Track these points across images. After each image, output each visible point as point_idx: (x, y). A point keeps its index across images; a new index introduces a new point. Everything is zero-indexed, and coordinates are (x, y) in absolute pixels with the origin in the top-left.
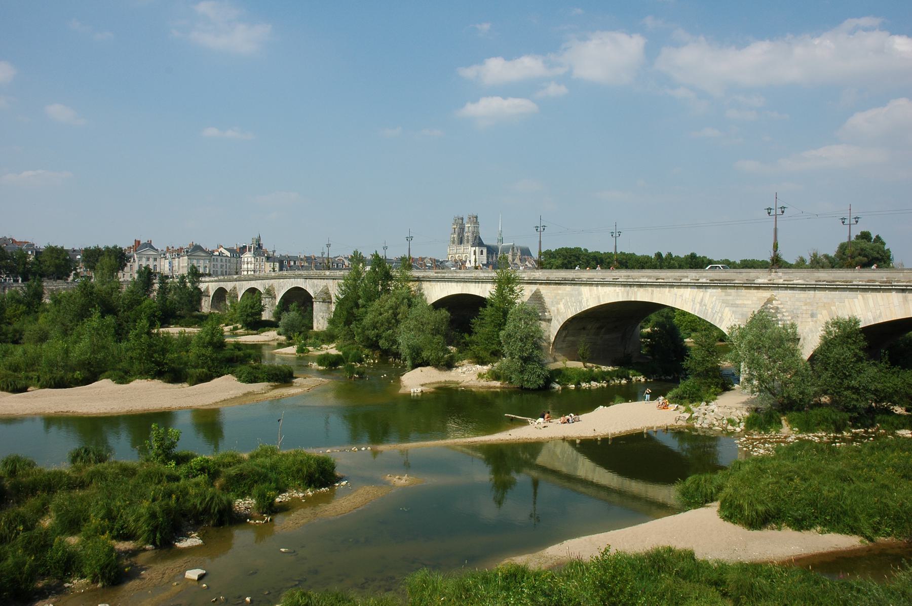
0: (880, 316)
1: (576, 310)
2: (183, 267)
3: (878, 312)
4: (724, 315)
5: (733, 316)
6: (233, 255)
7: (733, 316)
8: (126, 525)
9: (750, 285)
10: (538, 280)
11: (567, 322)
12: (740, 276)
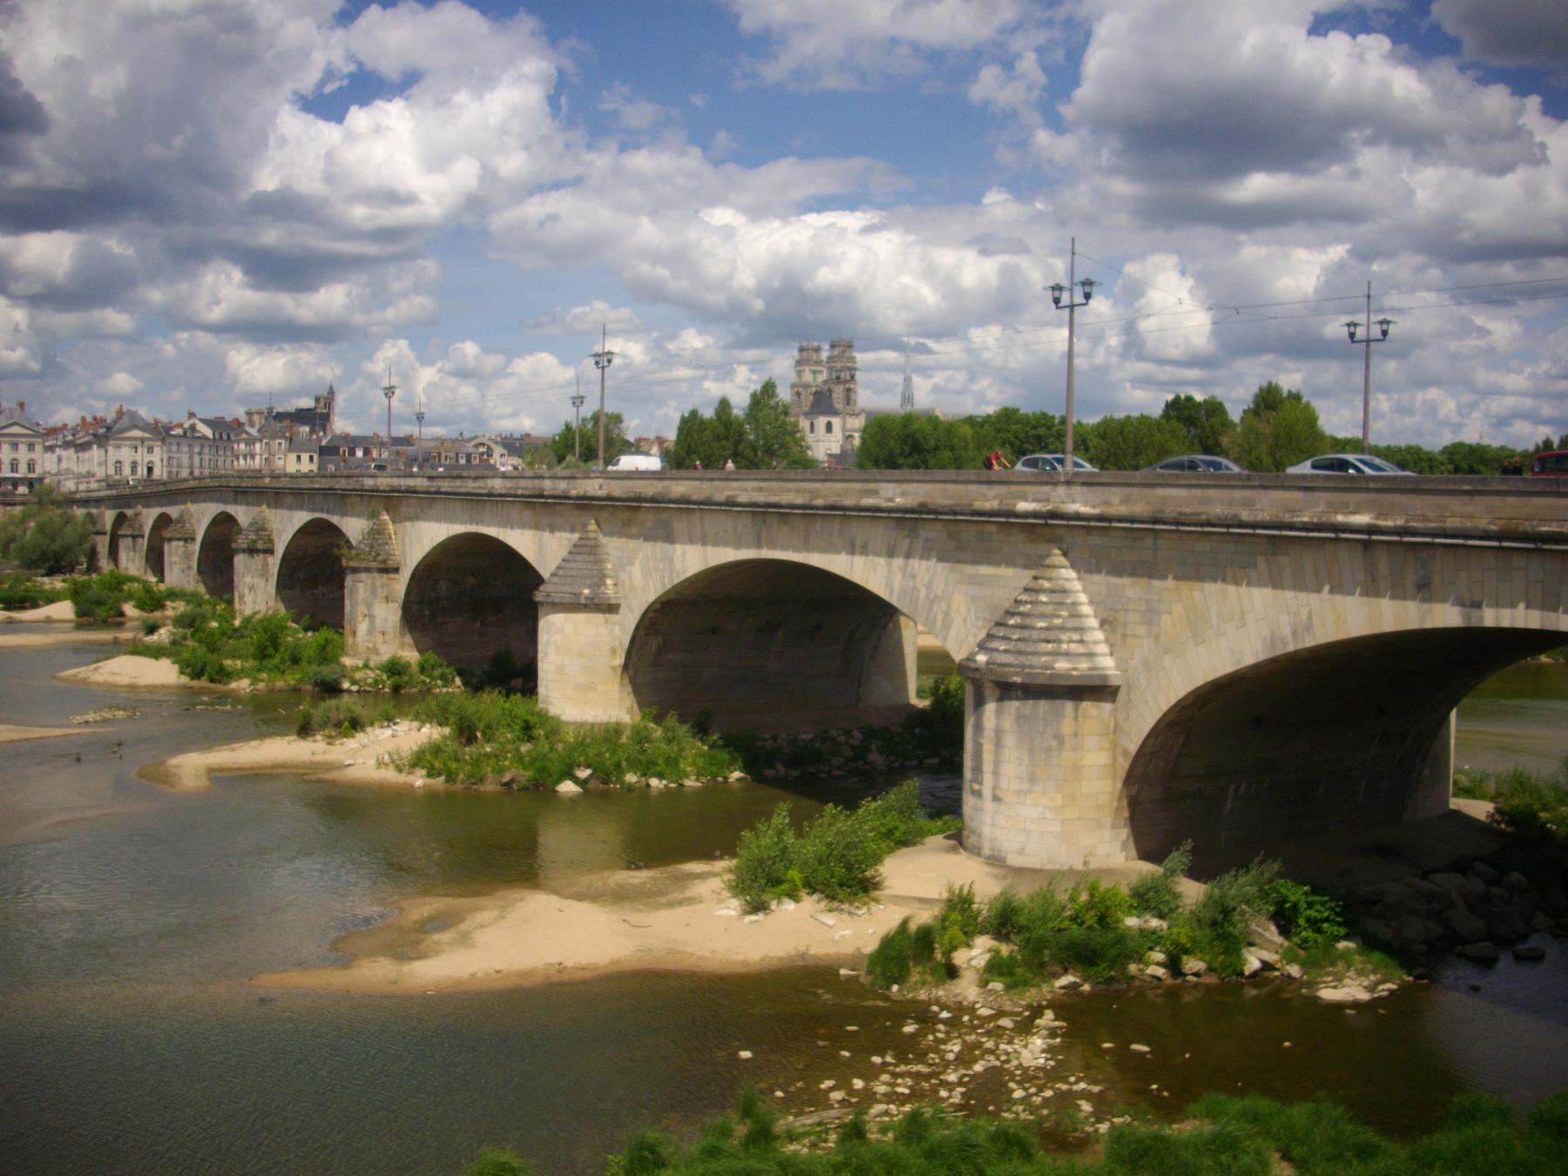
0: (1309, 627)
1: (663, 583)
2: (978, 476)
3: (1304, 614)
4: (954, 606)
5: (972, 610)
6: (221, 435)
7: (972, 610)
8: (113, 950)
9: (1428, 540)
10: (968, 521)
11: (651, 614)
12: (789, 498)
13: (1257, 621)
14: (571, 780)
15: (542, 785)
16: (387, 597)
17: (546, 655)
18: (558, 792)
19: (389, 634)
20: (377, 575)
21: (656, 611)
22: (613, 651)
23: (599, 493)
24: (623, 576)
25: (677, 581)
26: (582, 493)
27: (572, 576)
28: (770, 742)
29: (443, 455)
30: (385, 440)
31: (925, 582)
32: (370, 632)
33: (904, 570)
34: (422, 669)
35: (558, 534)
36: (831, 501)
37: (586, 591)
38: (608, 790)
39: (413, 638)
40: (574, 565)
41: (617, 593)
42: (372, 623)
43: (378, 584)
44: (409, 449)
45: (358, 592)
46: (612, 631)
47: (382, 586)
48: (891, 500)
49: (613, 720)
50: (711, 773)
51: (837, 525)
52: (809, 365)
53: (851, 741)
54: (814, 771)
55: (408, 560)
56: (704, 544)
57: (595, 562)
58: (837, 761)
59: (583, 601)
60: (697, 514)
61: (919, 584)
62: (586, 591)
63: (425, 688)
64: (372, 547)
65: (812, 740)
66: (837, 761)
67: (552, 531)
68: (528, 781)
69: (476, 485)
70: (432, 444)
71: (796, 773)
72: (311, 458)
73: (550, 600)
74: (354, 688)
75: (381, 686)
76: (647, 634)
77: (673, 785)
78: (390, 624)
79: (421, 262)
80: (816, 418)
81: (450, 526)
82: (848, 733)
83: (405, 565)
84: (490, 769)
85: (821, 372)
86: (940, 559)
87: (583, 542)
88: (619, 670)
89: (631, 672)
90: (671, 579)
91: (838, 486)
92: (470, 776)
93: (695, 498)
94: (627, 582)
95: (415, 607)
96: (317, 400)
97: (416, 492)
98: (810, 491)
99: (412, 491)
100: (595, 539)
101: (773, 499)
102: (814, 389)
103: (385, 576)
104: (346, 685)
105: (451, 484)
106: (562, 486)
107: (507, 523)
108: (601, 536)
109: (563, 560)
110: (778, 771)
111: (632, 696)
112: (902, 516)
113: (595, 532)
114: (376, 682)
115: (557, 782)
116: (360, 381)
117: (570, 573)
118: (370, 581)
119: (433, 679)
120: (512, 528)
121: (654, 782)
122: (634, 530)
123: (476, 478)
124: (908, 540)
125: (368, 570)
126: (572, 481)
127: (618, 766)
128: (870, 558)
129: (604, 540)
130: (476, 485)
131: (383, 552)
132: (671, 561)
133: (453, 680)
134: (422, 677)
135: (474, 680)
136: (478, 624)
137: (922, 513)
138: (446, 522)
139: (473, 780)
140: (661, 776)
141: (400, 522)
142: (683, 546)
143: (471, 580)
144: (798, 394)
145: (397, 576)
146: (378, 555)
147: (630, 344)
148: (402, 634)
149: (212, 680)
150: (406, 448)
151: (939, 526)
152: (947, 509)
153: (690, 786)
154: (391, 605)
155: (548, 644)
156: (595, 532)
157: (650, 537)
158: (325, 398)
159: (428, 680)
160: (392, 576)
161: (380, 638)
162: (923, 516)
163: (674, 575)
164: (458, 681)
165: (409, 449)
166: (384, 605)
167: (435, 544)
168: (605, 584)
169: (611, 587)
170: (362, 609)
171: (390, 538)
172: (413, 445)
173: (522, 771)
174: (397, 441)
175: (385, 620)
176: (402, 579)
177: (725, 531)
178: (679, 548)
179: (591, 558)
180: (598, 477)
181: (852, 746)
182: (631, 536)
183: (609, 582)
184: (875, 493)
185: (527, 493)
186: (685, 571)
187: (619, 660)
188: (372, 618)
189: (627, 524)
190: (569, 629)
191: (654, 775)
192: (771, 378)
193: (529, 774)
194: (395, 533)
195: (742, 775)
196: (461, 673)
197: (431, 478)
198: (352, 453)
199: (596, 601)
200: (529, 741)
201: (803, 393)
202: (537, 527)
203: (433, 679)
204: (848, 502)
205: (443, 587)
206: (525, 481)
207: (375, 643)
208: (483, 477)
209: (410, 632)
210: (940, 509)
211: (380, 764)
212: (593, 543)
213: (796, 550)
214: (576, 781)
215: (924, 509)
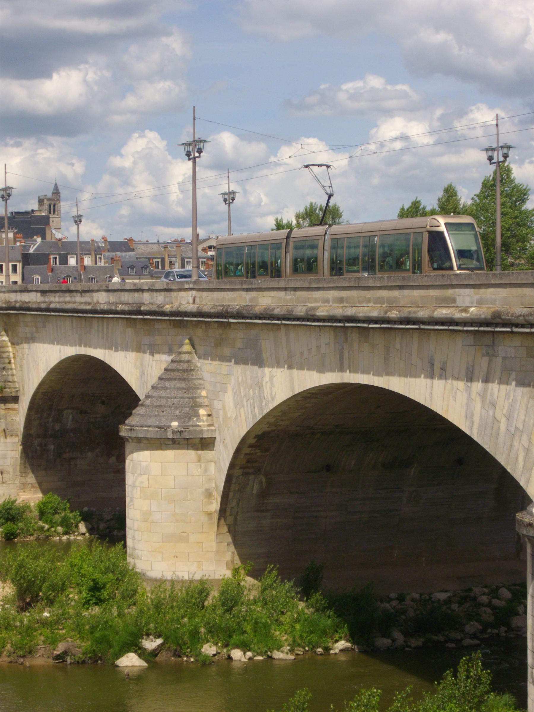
1: (254, 416)
11: (246, 450)
13: (163, 533)
14: (135, 652)
15: (100, 658)
17: (132, 500)
18: (118, 666)
19: (8, 473)
21: (251, 446)
22: (208, 494)
23: (191, 308)
24: (217, 405)
25: (266, 411)
26: (174, 309)
27: (160, 406)
28: (394, 603)
29: (167, 261)
30: (102, 245)
31: (505, 412)
33: (483, 396)
34: (42, 514)
35: (157, 356)
36: (405, 313)
37: (175, 424)
38: (181, 664)
39: (36, 477)
40: (162, 393)
41: (212, 425)
44: (127, 256)
46: (206, 470)
48: (465, 310)
49: (197, 577)
50: (310, 642)
51: (415, 340)
53: (495, 602)
54: (442, 639)
55: (26, 389)
56: (290, 367)
57: (187, 390)
58: (472, 627)
59: (170, 435)
60: (283, 331)
61: (498, 416)
62: (175, 424)
63: (42, 536)
65: (448, 602)
66: (472, 627)
67: (152, 354)
68: (85, 653)
69: (83, 300)
70: (155, 248)
71: (416, 642)
72: (15, 268)
73: (134, 435)
76: (245, 474)
77: (260, 658)
78: (9, 461)
79: (165, 40)
82: (494, 593)
83: (24, 394)
84: (42, 638)
86: (521, 383)
87: (174, 366)
88: (216, 516)
89: (231, 519)
90: (261, 409)
91: (417, 293)
92: (17, 647)
93: (277, 311)
94: (221, 413)
95: (37, 442)
96: (41, 201)
97: (29, 309)
98: (389, 301)
99: (25, 308)
100: (188, 361)
101: (350, 312)
105: (61, 300)
106: (160, 299)
107: (111, 346)
108: (195, 359)
109: (153, 387)
110: (394, 641)
111: (232, 548)
112: (476, 329)
113: (189, 353)
115: (119, 655)
116: (106, 178)
117: (159, 402)
119: (53, 524)
120: (116, 350)
121: (237, 654)
122: (226, 351)
123: (84, 292)
124: (486, 359)
126: (168, 294)
127: (195, 634)
128: (449, 381)
129: (199, 363)
132: (260, 386)
133: (77, 526)
134: (41, 523)
135: (102, 526)
137: (497, 325)
138: (58, 344)
139: (21, 653)
140: (245, 647)
141: (18, 344)
142: (270, 369)
143: (101, 409)
145: (16, 406)
147: (412, 124)
148: (23, 474)
150: (124, 254)
151: (517, 341)
152: (521, 320)
153: (280, 659)
154: (9, 440)
155: (133, 486)
156: (189, 353)
157: (240, 361)
158: (48, 200)
159: (47, 527)
162: (498, 329)
163: (264, 404)
164: (82, 528)
165: (127, 256)
167: (49, 369)
168: (197, 415)
169: (205, 418)
171: (10, 363)
172: (133, 250)
173: (78, 642)
174: (115, 246)
176: (21, 409)
177: (310, 350)
178: (267, 370)
179: (183, 385)
180: (192, 289)
181: (494, 608)
182: (223, 359)
183: (202, 412)
184: (451, 301)
185: (126, 308)
186: (273, 398)
187: (215, 506)
189: (219, 343)
190: (155, 469)
191: (237, 647)
193: (86, 645)
194: (14, 357)
195: (349, 645)
196: (86, 518)
197: (43, 292)
198: (64, 261)
199: (186, 435)
200: (96, 604)
202: (139, 349)
203: (53, 524)
204: (422, 314)
205: (69, 416)
206: (126, 294)
208: (89, 291)
209: (33, 472)
210: (515, 321)
212: (185, 366)
213: (377, 374)
214: (141, 652)
215: (498, 320)
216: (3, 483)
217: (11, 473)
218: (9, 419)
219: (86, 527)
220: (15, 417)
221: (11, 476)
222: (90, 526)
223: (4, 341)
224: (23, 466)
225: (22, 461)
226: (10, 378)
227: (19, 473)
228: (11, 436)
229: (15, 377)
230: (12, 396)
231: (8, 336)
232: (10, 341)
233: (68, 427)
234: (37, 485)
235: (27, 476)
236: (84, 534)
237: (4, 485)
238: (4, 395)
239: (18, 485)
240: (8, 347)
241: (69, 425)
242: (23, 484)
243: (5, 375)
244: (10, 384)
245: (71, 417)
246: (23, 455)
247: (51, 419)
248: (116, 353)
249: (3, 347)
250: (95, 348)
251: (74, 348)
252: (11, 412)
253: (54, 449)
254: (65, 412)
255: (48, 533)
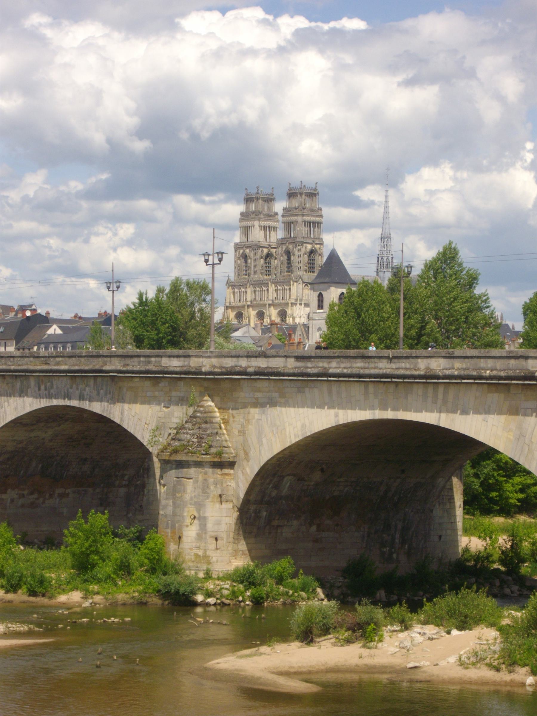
16: (220, 496)
19: (222, 539)
20: (210, 470)
32: (200, 537)
39: (247, 544)
42: (203, 527)
43: (211, 480)
45: (184, 491)
47: (216, 484)
52: (259, 220)
63: (289, 601)
64: (200, 438)
74: (211, 600)
75: (240, 598)
78: (223, 527)
80: (325, 290)
81: (341, 412)
85: (275, 229)
102: (265, 251)
103: (219, 471)
104: (200, 598)
114: (234, 594)
118: (201, 478)
125: (199, 464)
130: (393, 366)
131: (214, 444)
136: (314, 528)
144: (245, 257)
145: (232, 472)
146: (211, 446)
148: (236, 540)
149: (33, 593)
154: (225, 505)
159: (291, 592)
160: (226, 471)
161: (212, 544)
166: (218, 505)
170: (190, 511)
175: (218, 523)
188: (202, 520)
192: (450, 243)
201: (252, 255)
202: (514, 411)
207: (205, 551)
209: (245, 538)
211: (461, 663)
216: (217, 549)
217: (225, 540)
218: (225, 485)
219: (324, 593)
220: (230, 482)
221: (225, 543)
222: (327, 593)
223: (211, 406)
224: (237, 532)
225: (237, 528)
226: (225, 444)
227: (231, 540)
228: (227, 501)
229: (229, 442)
230: (229, 461)
231: (213, 401)
232: (216, 406)
233: (282, 494)
234: (247, 552)
235: (239, 543)
236: (323, 600)
237: (218, 551)
238: (223, 460)
239: (231, 551)
240: (215, 412)
241: (284, 491)
242: (235, 551)
243: (219, 440)
244: (225, 449)
245: (288, 484)
246: (239, 521)
247: (271, 486)
248: (463, 417)
249: (210, 412)
250: (465, 412)
251: (332, 412)
252: (227, 477)
253: (266, 515)
254: (286, 478)
255: (292, 598)
